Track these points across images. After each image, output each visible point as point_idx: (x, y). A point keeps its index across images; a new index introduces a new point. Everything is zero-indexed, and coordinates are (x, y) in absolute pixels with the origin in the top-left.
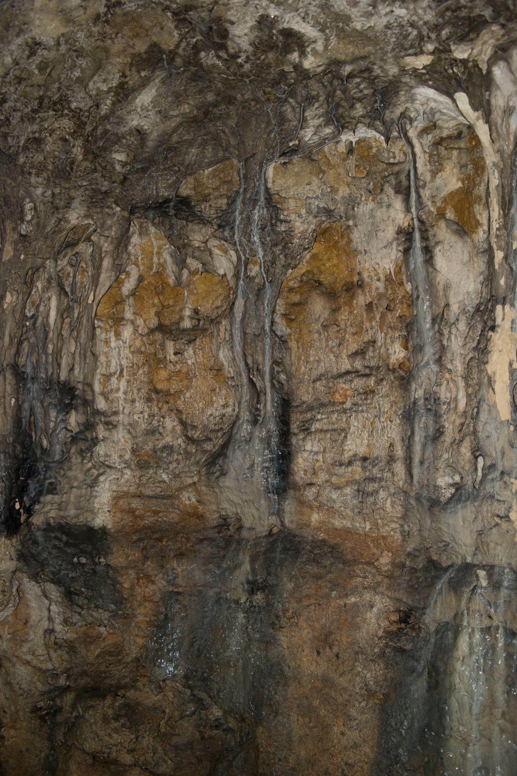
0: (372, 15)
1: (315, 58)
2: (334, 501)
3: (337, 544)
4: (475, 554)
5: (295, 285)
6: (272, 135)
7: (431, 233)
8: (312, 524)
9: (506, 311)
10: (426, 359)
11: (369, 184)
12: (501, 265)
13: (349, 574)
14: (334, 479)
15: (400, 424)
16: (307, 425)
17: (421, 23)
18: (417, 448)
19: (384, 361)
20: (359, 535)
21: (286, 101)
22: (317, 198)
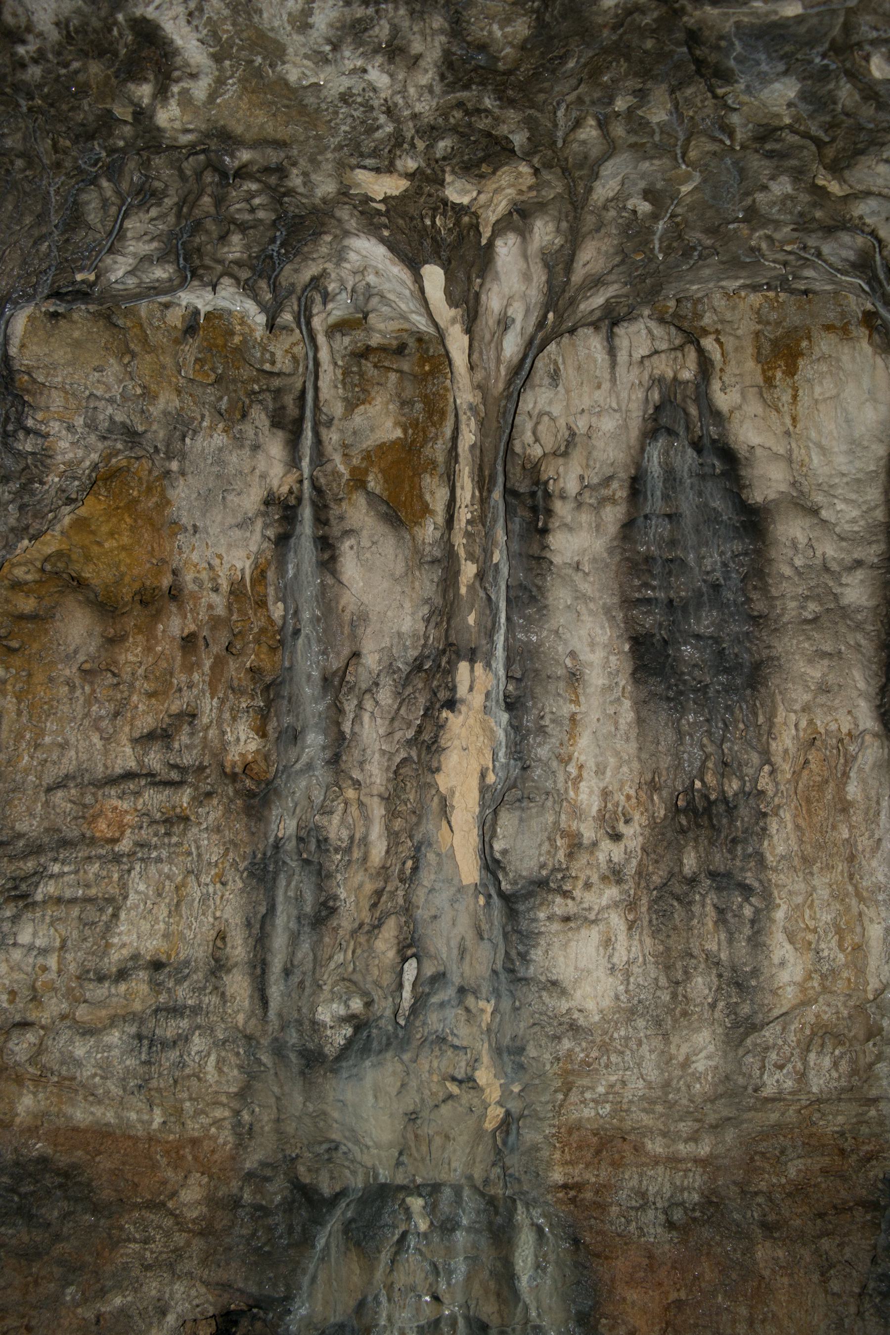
0: (327, 61)
1: (183, 112)
2: (79, 1064)
3: (74, 1166)
4: (399, 1164)
5: (29, 577)
6: (44, 247)
7: (335, 511)
8: (18, 1120)
9: (477, 674)
10: (304, 759)
11: (221, 398)
12: (471, 588)
13: (110, 1236)
14: (82, 1013)
15: (242, 891)
16: (24, 887)
17: (407, 113)
18: (279, 941)
19: (214, 755)
20: (135, 1139)
21: (94, 181)
22: (111, 401)
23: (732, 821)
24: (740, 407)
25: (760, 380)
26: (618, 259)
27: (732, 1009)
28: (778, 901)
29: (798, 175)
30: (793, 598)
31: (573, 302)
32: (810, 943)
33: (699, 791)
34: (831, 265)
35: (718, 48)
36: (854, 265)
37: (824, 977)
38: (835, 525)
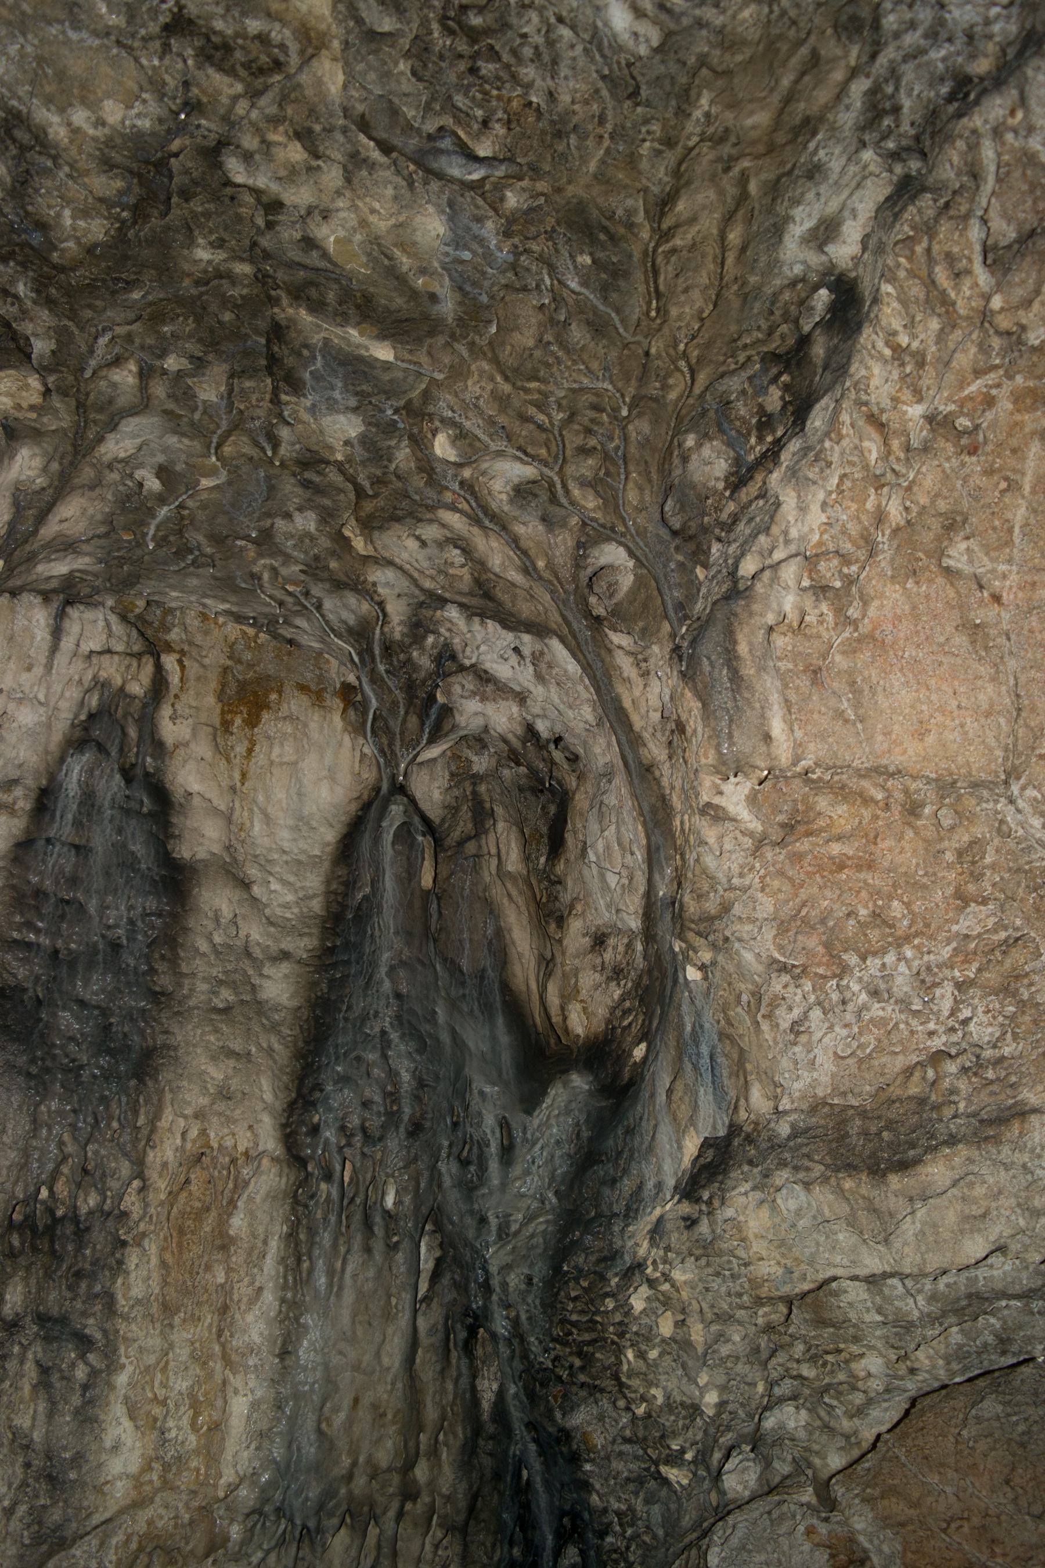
23: (80, 1247)
24: (186, 745)
25: (217, 721)
26: (102, 530)
27: (37, 1517)
28: (123, 1360)
29: (326, 516)
30: (205, 979)
31: (32, 559)
32: (155, 1420)
33: (43, 1202)
34: (327, 622)
35: (299, 354)
36: (350, 631)
37: (166, 1467)
38: (266, 906)
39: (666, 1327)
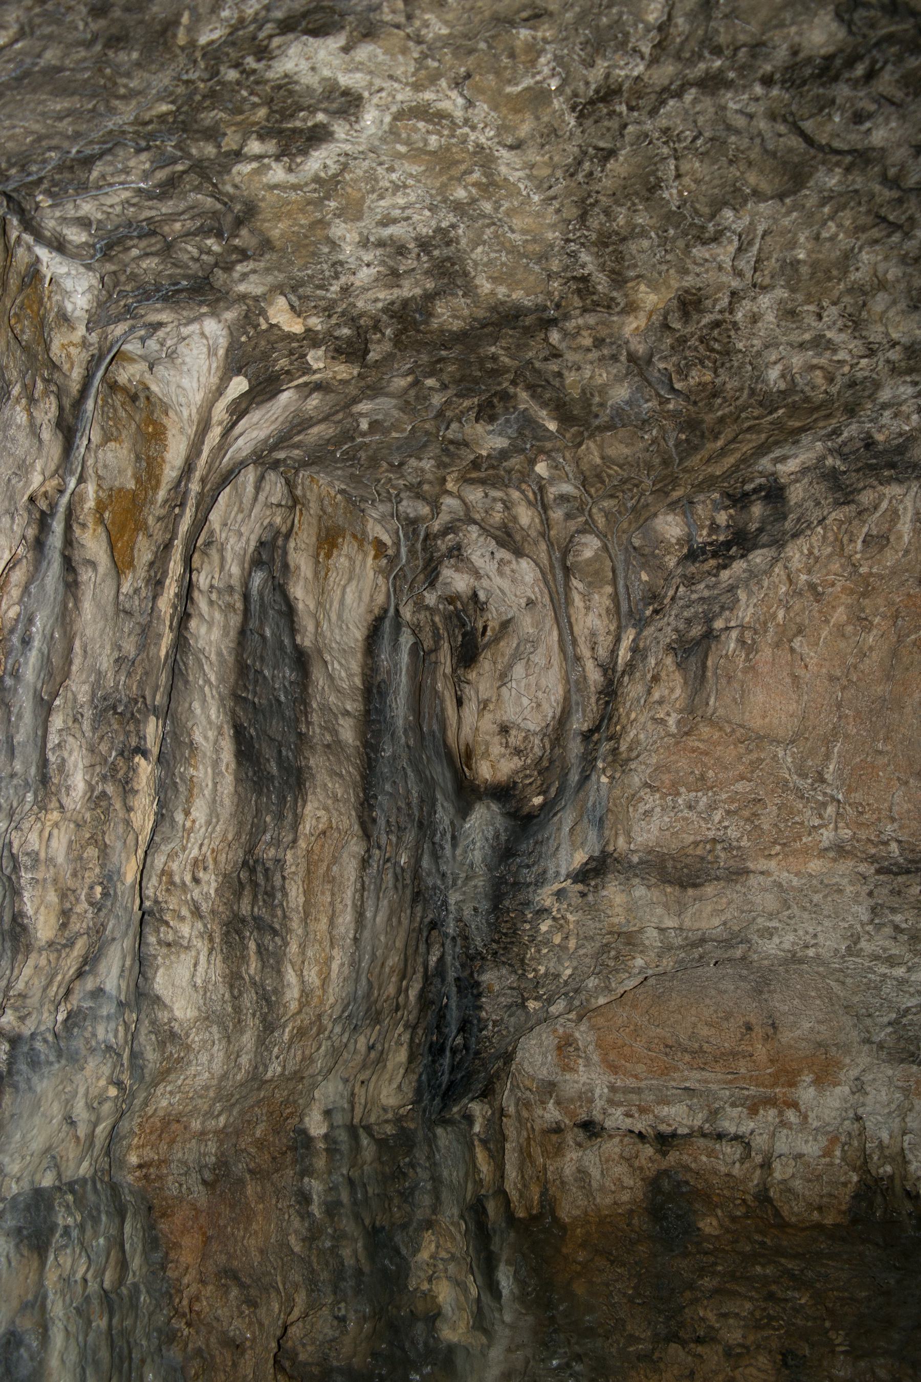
36: (407, 518)
39: (557, 940)
